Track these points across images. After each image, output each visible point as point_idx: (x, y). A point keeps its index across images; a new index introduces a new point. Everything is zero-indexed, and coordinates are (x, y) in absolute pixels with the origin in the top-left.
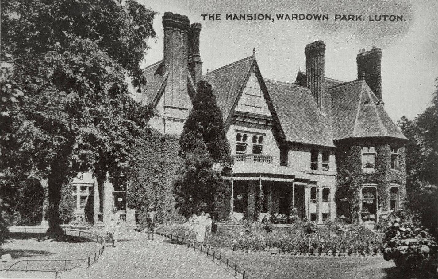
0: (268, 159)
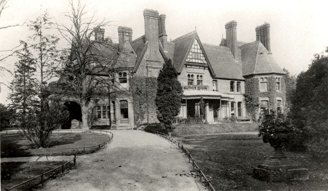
0: (205, 88)
